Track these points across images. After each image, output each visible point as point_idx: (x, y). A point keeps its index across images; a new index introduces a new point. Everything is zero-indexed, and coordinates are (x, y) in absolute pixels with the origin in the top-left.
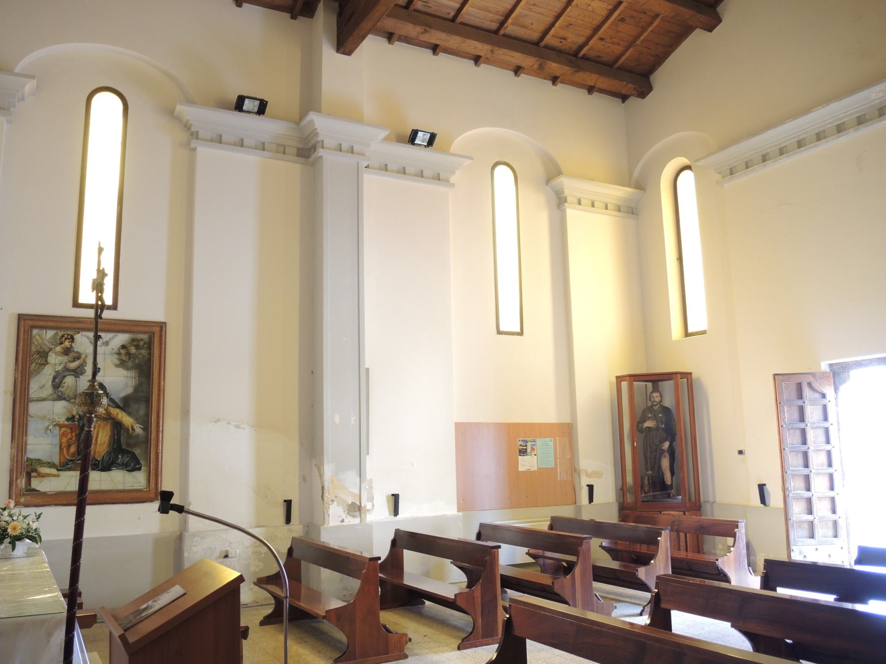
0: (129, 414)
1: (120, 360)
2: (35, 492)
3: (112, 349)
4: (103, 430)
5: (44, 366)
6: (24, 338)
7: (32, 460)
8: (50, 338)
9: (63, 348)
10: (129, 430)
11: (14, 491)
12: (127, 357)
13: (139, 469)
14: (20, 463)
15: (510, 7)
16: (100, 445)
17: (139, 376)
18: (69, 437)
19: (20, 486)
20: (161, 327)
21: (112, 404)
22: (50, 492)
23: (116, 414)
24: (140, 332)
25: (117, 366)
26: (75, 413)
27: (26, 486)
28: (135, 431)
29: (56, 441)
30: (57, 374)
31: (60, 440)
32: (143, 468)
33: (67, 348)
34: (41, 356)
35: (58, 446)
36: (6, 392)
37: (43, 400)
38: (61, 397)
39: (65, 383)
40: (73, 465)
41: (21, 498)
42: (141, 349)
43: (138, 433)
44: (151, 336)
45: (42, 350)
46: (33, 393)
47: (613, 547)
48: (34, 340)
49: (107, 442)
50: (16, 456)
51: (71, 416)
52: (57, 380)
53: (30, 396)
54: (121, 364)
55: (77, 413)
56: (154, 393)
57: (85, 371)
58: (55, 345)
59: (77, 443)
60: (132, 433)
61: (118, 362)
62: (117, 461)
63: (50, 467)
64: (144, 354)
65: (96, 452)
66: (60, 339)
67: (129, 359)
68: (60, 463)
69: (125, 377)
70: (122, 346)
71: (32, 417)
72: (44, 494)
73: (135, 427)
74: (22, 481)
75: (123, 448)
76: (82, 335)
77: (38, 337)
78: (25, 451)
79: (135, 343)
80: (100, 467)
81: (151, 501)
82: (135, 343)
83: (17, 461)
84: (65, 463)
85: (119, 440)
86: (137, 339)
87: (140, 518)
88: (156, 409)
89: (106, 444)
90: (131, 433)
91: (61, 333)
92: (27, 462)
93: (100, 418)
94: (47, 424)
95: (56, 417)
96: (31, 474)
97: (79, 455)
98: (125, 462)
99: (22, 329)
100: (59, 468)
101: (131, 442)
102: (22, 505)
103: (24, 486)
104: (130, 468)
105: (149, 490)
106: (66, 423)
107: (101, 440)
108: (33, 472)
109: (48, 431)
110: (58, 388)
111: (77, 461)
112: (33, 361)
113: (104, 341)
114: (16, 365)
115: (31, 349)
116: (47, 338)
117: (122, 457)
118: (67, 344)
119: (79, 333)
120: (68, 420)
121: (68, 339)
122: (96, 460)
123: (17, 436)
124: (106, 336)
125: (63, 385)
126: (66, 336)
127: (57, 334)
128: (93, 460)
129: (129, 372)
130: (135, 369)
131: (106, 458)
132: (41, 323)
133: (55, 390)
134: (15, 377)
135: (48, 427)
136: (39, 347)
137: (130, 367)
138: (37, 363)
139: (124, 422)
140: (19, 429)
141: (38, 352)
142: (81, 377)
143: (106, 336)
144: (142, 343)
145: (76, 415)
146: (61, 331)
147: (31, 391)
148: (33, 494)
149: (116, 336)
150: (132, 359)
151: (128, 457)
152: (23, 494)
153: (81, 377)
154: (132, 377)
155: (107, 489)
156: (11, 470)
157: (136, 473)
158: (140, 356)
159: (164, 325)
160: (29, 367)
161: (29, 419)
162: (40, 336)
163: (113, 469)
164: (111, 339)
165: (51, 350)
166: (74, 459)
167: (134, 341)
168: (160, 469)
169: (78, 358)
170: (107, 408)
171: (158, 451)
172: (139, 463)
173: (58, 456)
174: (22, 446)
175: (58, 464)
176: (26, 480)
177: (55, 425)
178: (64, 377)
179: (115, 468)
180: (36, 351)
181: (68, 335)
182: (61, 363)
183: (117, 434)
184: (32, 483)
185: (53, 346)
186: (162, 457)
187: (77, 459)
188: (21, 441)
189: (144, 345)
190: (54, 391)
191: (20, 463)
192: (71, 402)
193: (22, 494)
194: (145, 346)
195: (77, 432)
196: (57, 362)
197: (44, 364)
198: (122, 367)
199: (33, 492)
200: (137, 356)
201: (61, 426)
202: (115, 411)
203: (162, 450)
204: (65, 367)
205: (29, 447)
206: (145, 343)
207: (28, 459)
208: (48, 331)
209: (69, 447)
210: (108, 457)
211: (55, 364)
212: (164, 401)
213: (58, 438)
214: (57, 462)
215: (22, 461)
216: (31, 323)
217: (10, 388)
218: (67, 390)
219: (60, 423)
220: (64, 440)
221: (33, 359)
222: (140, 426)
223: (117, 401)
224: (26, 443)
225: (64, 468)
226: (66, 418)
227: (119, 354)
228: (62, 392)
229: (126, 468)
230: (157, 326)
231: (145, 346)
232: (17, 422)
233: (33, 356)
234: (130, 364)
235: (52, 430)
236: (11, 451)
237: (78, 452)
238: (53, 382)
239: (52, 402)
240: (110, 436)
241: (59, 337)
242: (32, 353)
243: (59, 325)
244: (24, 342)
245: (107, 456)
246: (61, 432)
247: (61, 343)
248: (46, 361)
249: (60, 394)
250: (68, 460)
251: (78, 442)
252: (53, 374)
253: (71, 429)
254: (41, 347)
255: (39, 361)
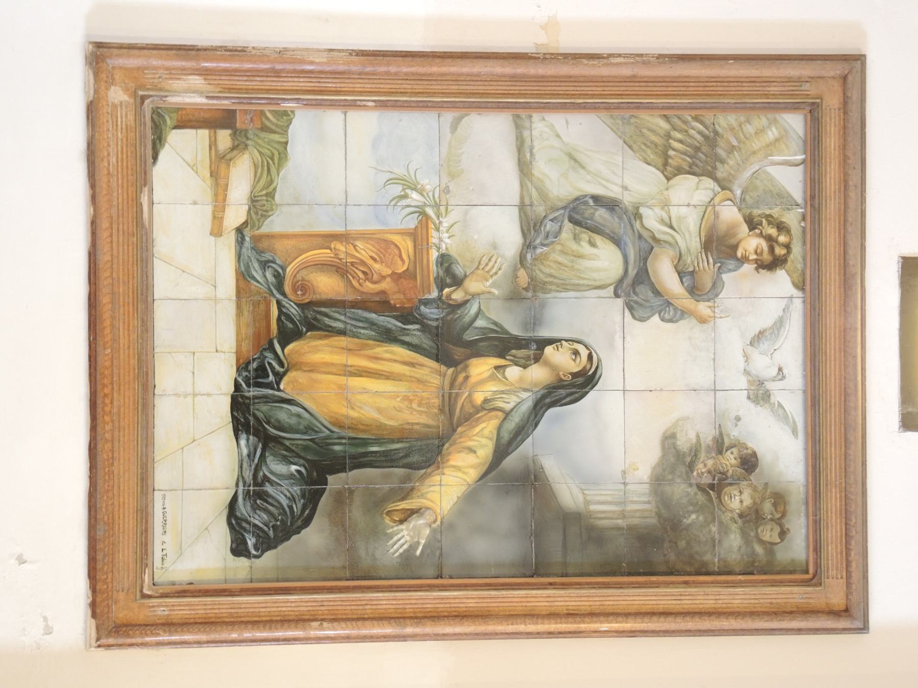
0: (471, 497)
1: (695, 452)
2: (149, 146)
3: (738, 419)
4: (406, 398)
5: (659, 161)
6: (768, 81)
7: (284, 130)
8: (772, 180)
9: (731, 230)
10: (403, 499)
11: (155, 62)
12: (706, 480)
13: (239, 549)
14: (270, 83)
15: (383, 576)
16: (343, 388)
17: (631, 528)
18: (377, 266)
19: (176, 84)
20: (846, 612)
21: (511, 425)
22: (151, 203)
23: (470, 444)
24: (816, 526)
25: (669, 439)
26: (473, 285)
27: (178, 109)
28: (401, 522)
29: (360, 221)
30: (626, 212)
31: (365, 236)
32: (243, 562)
33: (735, 247)
34: (697, 149)
35: (339, 229)
36: (550, 25)
37: (524, 167)
38: (537, 230)
39: (592, 244)
40: (264, 289)
41: (126, 90)
42: (744, 534)
43: (391, 537)
44: (807, 572)
45: (721, 152)
46: (552, 127)
47: (500, 467)
48: (760, 120)
49: (353, 414)
50: (299, 67)
51: (459, 271)
52: (601, 214)
53: (536, 116)
54: (679, 455)
55: (474, 296)
56: (562, 592)
57: (642, 320)
58: (743, 200)
59: (351, 297)
60: (389, 513)
61: (684, 442)
62: (274, 455)
63: (253, 201)
64: (726, 544)
65: (315, 376)
66: (767, 217)
67: (700, 487)
68: (270, 236)
69: (624, 472)
70: (754, 454)
71: (454, 127)
72: (143, 179)
73: (417, 522)
74: (200, 93)
75: (330, 478)
76: (791, 297)
77: (772, 134)
78: (319, 104)
79: (767, 507)
80: (252, 392)
81: (93, 605)
82: (767, 507)
83: (277, 73)
84: (268, 256)
85: (360, 461)
86: (784, 515)
87: (21, 560)
88: (493, 605)
89: (344, 411)
90: (392, 506)
91: (792, 219)
92: (274, 112)
93: (452, 385)
94: (429, 182)
95: (455, 215)
96: (224, 127)
97: (301, 306)
98: (268, 488)
99: (806, 70)
100: (247, 233)
101: (356, 513)
102: (96, 91)
103: (174, 100)
104: (243, 509)
105: (145, 596)
106: (434, 255)
107: (365, 391)
108: (234, 135)
109: (397, 190)
110: (572, 220)
111: (279, 303)
112: (676, 120)
113: (770, 386)
114: (660, 56)
115: (725, 108)
116: (772, 170)
117: (291, 476)
118: (752, 244)
119: (800, 286)
120: (445, 260)
121: (772, 250)
122: (279, 377)
123: (382, 69)
124: (792, 391)
125: (585, 236)
126: (782, 239)
127: (789, 203)
128: (281, 364)
129: (646, 488)
130: (659, 515)
131: (291, 414)
132: (831, 142)
133: (564, 208)
134: (610, 55)
135: (415, 189)
136: (735, 143)
137: (668, 489)
138: (668, 136)
139: (437, 478)
140: (407, 77)
141: (712, 139)
142: (620, 302)
143: (792, 391)
144: (769, 533)
145: (466, 293)
146: (804, 218)
147: (557, 119)
148: (143, 137)
149: (794, 432)
150: (701, 498)
151: (292, 499)
152: (143, 98)
153: (620, 302)
154: (623, 503)
155: (157, 421)
156: (243, 50)
157: (221, 535)
158: (714, 529)
159: (858, 624)
160: (650, 107)
161: (448, 117)
162: (777, 140)
163: (243, 442)
164: (780, 412)
165: (724, 185)
166: (287, 288)
167: (775, 505)
168: (234, 636)
169: (694, 291)
170: (495, 409)
171: (315, 624)
172: (266, 544)
173: (298, 229)
174: (337, 93)
175: (264, 230)
176: (199, 109)
177: (423, 214)
178: (617, 241)
179: (245, 451)
180: (716, 133)
181: (788, 246)
182: (671, 227)
183: (385, 454)
184: (189, 133)
185: (738, 192)
186: (287, 640)
187: (285, 302)
188: (358, 87)
189: (761, 542)
190: (561, 204)
191: (270, 83)
192: (515, 270)
193: (141, 93)
194: (759, 549)
195: (396, 299)
196: (674, 211)
197: (666, 164)
198: (663, 456)
199: (150, 137)
200: (713, 521)
201: (419, 236)
202: (484, 441)
203: (319, 640)
204: (657, 241)
205: (333, 119)
206: (770, 547)
207: (286, 116)
208: (801, 167)
209: (340, 269)
210: (293, 421)
211: (665, 205)
212: (799, 631)
213: (374, 226)
214: (275, 224)
215: (277, 91)
216: (832, 101)
217: (568, 42)
218: (563, 252)
219: (433, 233)
220: (364, 251)
221: (685, 122)
222: (423, 542)
223: (526, 447)
224: (354, 105)
225: (247, 251)
226: (453, 253)
227: (719, 446)
228: (557, 234)
229: (247, 494)
230: (848, 594)
231: (759, 549)
232: (435, 69)
233: (696, 119)
234: (680, 490)
235: (404, 202)
236: (319, 50)
237: (311, 303)
238: (596, 198)
239: (516, 200)
240: (380, 426)
241: (775, 212)
242: (709, 117)
243: (831, 208)
244: (753, 81)
245: (299, 416)
246: (397, 239)
247: (752, 224)
248: (679, 171)
249: (549, 226)
250: (284, 269)
251: (355, 305)
252: (627, 199)
253: (409, 275)
254: (732, 149)
255: (676, 145)
